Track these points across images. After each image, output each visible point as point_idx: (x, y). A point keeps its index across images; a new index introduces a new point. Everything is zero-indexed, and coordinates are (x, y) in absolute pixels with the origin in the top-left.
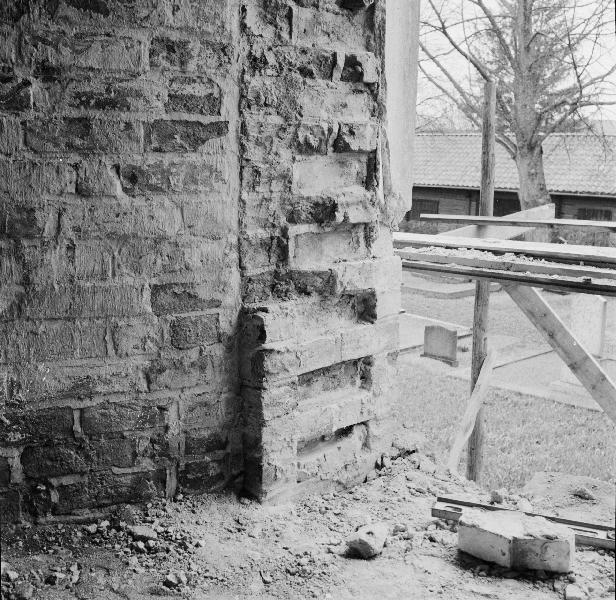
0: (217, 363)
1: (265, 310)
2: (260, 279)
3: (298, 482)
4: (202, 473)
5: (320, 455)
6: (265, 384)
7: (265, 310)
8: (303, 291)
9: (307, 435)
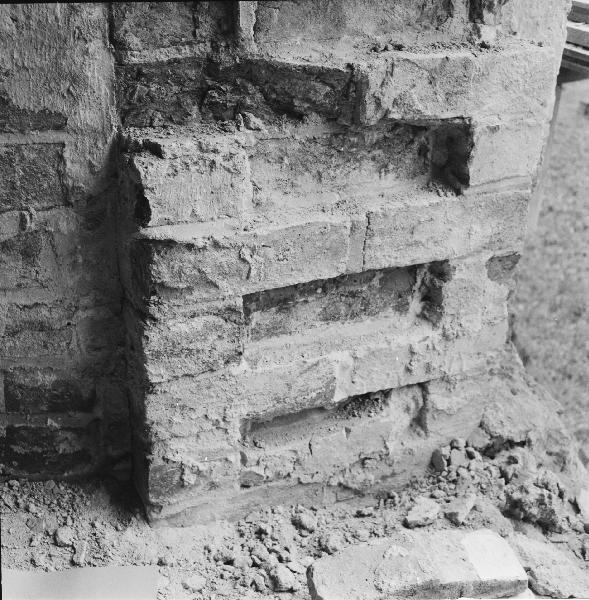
0: (63, 246)
1: (156, 151)
2: (167, 72)
3: (244, 486)
4: (41, 446)
5: (300, 445)
6: (153, 309)
7: (156, 151)
8: (284, 109)
9: (264, 407)
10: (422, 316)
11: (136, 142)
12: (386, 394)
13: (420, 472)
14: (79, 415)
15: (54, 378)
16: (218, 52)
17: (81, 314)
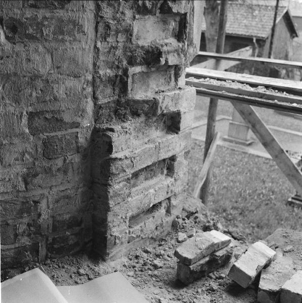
1: (112, 130)
5: (142, 224)
7: (112, 130)
8: (135, 114)
10: (167, 175)
11: (103, 129)
12: (160, 203)
13: (169, 229)
14: (77, 228)
15: (70, 215)
16: (121, 98)
17: (80, 190)
